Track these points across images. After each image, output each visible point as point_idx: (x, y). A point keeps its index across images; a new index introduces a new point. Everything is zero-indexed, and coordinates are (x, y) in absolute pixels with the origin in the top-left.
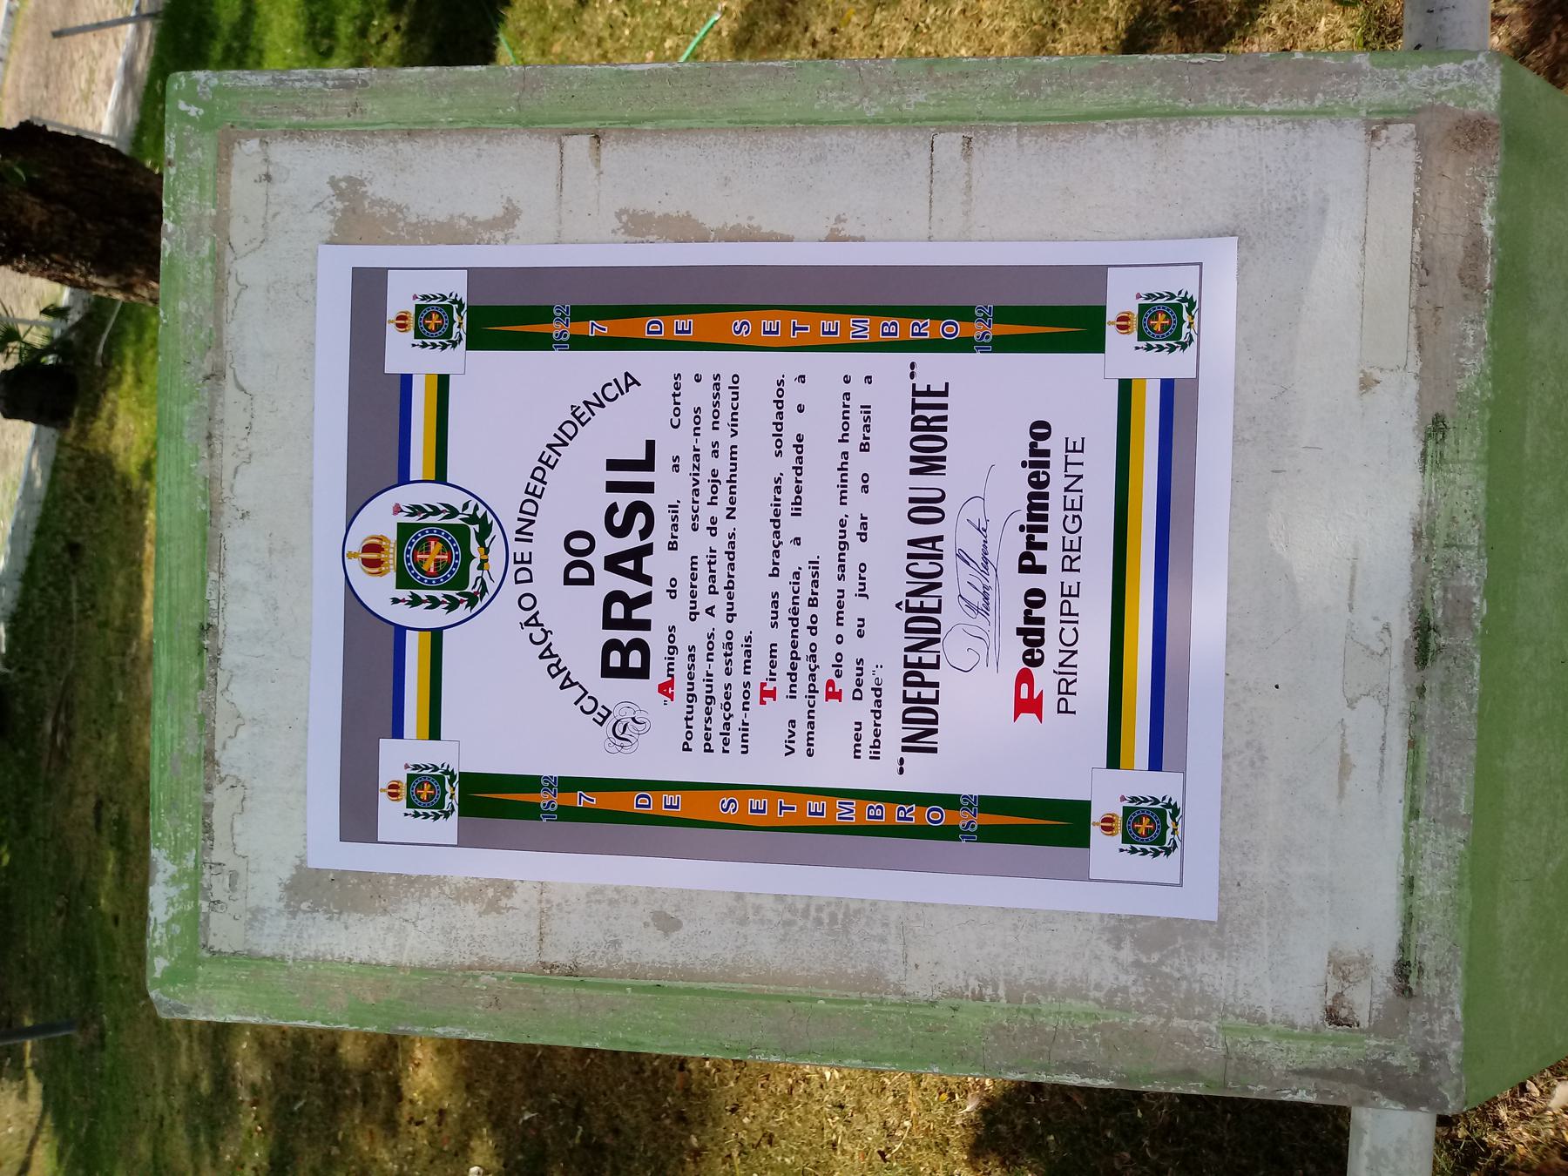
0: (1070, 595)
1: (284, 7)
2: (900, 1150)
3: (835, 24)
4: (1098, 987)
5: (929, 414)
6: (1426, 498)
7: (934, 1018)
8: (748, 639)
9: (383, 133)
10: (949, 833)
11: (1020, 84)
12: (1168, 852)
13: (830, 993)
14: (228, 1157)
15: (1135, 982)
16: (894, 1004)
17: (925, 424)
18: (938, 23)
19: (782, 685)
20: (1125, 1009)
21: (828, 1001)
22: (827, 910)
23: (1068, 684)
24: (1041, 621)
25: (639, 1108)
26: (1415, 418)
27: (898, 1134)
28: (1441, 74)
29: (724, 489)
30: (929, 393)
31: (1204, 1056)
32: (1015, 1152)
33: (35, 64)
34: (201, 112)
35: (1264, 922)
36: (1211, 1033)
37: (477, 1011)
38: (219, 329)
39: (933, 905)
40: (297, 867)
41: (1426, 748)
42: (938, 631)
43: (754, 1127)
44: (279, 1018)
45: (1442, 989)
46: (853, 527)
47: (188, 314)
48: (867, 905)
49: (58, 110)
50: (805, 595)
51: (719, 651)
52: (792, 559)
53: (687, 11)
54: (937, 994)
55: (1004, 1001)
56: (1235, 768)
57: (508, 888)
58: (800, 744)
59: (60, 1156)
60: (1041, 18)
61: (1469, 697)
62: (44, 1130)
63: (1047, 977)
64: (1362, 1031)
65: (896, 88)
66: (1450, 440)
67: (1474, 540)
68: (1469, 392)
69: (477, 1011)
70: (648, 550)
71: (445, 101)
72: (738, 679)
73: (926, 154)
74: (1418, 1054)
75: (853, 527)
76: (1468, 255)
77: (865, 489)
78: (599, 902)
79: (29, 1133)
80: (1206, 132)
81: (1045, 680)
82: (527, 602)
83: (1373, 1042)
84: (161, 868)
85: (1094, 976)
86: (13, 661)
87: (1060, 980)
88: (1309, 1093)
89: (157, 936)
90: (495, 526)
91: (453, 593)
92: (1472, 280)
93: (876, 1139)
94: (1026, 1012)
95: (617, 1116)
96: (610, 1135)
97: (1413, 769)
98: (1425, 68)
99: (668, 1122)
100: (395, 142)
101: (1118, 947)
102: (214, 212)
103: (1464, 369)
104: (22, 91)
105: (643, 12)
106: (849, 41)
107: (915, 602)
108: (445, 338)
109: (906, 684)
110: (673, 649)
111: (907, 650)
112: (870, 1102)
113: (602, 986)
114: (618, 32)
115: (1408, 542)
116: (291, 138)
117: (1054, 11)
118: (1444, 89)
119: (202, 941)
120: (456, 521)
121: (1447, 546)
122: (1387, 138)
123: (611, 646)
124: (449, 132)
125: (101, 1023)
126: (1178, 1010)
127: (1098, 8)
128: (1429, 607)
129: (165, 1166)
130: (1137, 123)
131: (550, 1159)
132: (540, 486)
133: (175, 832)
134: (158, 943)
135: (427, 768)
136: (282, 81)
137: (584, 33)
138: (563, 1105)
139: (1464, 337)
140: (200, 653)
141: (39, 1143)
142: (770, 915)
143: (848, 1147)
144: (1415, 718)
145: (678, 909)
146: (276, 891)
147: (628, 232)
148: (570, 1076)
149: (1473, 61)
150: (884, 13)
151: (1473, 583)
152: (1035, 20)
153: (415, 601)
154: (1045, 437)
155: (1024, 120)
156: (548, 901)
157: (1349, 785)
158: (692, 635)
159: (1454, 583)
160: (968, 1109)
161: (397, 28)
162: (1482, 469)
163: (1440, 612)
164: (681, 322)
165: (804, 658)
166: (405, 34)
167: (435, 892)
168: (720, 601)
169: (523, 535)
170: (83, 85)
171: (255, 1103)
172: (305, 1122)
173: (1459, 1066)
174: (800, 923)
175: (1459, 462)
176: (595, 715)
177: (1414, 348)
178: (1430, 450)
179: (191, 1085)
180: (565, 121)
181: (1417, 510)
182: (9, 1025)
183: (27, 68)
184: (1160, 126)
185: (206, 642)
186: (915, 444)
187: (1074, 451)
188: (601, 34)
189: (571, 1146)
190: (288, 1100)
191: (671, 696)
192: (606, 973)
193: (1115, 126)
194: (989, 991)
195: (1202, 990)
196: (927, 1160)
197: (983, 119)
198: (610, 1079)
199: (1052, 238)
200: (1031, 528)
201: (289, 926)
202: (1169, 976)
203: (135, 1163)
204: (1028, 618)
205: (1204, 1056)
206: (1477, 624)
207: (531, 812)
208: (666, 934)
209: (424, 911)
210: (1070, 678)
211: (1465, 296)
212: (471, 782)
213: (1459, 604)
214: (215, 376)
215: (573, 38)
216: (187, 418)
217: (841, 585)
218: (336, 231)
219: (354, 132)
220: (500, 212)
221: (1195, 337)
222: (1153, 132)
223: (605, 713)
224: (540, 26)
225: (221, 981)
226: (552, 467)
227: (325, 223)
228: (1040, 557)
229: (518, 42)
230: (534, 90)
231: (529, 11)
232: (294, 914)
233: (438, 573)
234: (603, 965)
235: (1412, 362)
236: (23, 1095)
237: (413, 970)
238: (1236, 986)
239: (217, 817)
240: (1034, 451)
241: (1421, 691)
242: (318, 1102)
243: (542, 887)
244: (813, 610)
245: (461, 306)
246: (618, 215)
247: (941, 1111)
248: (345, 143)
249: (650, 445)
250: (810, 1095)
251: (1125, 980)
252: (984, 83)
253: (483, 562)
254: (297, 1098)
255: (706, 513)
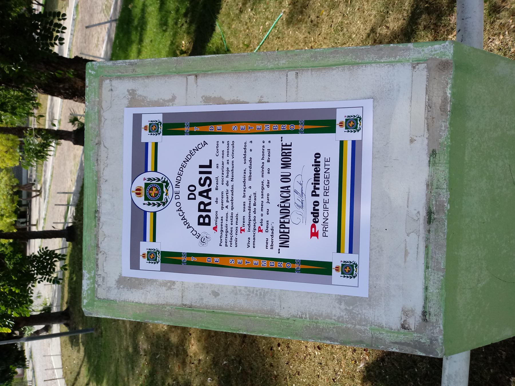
0: (326, 203)
1: (153, 16)
2: (339, 379)
3: (318, 15)
4: (335, 316)
5: (287, 151)
6: (430, 174)
7: (289, 323)
8: (237, 215)
9: (141, 77)
10: (292, 270)
11: (312, 57)
12: (354, 277)
13: (260, 315)
14: (137, 372)
15: (345, 315)
16: (277, 319)
17: (285, 154)
18: (350, 13)
19: (246, 228)
20: (343, 322)
21: (259, 317)
22: (259, 292)
23: (326, 228)
24: (318, 210)
25: (259, 361)
26: (427, 151)
27: (339, 373)
28: (435, 48)
29: (230, 173)
30: (286, 145)
31: (366, 337)
32: (376, 381)
33: (82, 36)
34: (95, 73)
35: (383, 298)
36: (368, 330)
37: (166, 317)
38: (99, 131)
39: (288, 291)
40: (119, 276)
41: (431, 247)
42: (289, 213)
43: (293, 369)
44: (115, 317)
45: (436, 320)
46: (265, 183)
47: (92, 127)
48: (270, 290)
49: (89, 50)
50: (252, 203)
51: (229, 218)
52: (249, 192)
53: (273, 13)
54: (289, 316)
55: (308, 319)
56: (374, 253)
57: (173, 283)
58: (251, 245)
59: (89, 370)
60: (384, 10)
61: (444, 233)
62: (84, 362)
63: (320, 312)
64: (412, 331)
65: (277, 59)
66: (437, 157)
67: (445, 186)
68: (443, 142)
69: (166, 317)
70: (210, 190)
71: (157, 68)
72: (234, 226)
73: (286, 77)
74: (430, 339)
75: (265, 183)
76: (442, 102)
77: (269, 173)
78: (198, 287)
79: (80, 363)
80: (365, 69)
81: (319, 227)
82: (178, 205)
83: (416, 335)
84: (85, 275)
85: (334, 313)
86: (77, 218)
87: (324, 313)
88: (396, 349)
89: (84, 294)
90: (170, 183)
91: (159, 202)
92: (443, 109)
93: (332, 375)
94: (314, 322)
95: (252, 364)
96: (250, 370)
97: (427, 254)
98: (430, 47)
99: (267, 366)
100: (144, 79)
101: (340, 305)
102: (98, 100)
103: (441, 136)
104: (78, 44)
105: (259, 14)
106: (323, 20)
107: (283, 205)
108: (157, 132)
109: (280, 228)
110: (217, 218)
111: (280, 218)
112: (330, 363)
113: (199, 311)
114: (252, 20)
115: (425, 187)
116: (117, 79)
117: (388, 8)
118: (435, 53)
119: (96, 296)
120: (160, 182)
121: (437, 188)
122: (418, 68)
123: (200, 216)
124: (157, 76)
125: (101, 330)
126: (358, 323)
127: (402, 6)
128: (431, 206)
129: (119, 374)
130: (345, 67)
131: (232, 376)
132: (182, 172)
133: (89, 266)
134: (85, 295)
135: (348, 262)
136: (115, 64)
137: (241, 21)
138: (235, 360)
139: (442, 127)
140: (95, 218)
141: (83, 366)
142: (243, 292)
143: (323, 377)
144: (427, 239)
145: (219, 290)
146: (114, 283)
147: (205, 102)
148: (237, 350)
149: (445, 44)
150: (334, 11)
151: (445, 199)
152: (381, 11)
153: (149, 204)
154: (319, 157)
155: (313, 67)
156: (184, 287)
157: (408, 259)
158: (222, 213)
159: (439, 199)
160: (361, 366)
161: (186, 22)
162: (447, 165)
163: (435, 208)
164: (219, 127)
165: (252, 220)
166: (188, 24)
167: (155, 284)
168: (229, 204)
169: (177, 186)
170: (96, 42)
171: (145, 355)
172: (160, 362)
173: (442, 343)
174: (252, 295)
175: (440, 163)
176: (196, 236)
177: (426, 130)
178: (431, 160)
179: (127, 350)
180: (188, 72)
181: (428, 178)
182: (75, 329)
183: (79, 37)
184: (351, 67)
185: (97, 215)
186: (282, 160)
187: (327, 161)
188: (247, 21)
189: (238, 373)
190: (155, 354)
191: (216, 231)
192: (199, 307)
193: (338, 68)
194: (304, 316)
195: (365, 318)
196: (348, 382)
197: (301, 67)
198: (250, 352)
199: (321, 100)
200: (315, 184)
201: (118, 292)
202: (355, 313)
203: (110, 373)
204: (314, 209)
205: (366, 337)
206: (446, 211)
207: (180, 262)
208: (215, 297)
209: (152, 289)
210: (326, 227)
211: (442, 114)
212: (164, 254)
213: (441, 206)
214: (99, 144)
215: (238, 23)
216: (92, 155)
217: (262, 200)
218: (129, 104)
219: (133, 77)
220: (171, 98)
221: (361, 128)
222: (349, 69)
223: (199, 235)
224: (228, 19)
225: (101, 306)
226: (185, 167)
227: (126, 102)
228: (318, 192)
229: (222, 25)
230: (180, 64)
231: (225, 15)
232: (119, 289)
233: (155, 196)
234: (199, 305)
235: (426, 134)
236: (78, 351)
237: (149, 305)
238: (374, 316)
239: (100, 262)
240: (316, 162)
241: (429, 231)
242: (164, 356)
243: (183, 283)
244: (255, 207)
245: (161, 123)
246: (202, 97)
247: (352, 367)
248: (131, 80)
249: (211, 161)
250: (311, 360)
251: (343, 314)
252: (302, 57)
253: (167, 193)
254: (157, 354)
255: (225, 180)
